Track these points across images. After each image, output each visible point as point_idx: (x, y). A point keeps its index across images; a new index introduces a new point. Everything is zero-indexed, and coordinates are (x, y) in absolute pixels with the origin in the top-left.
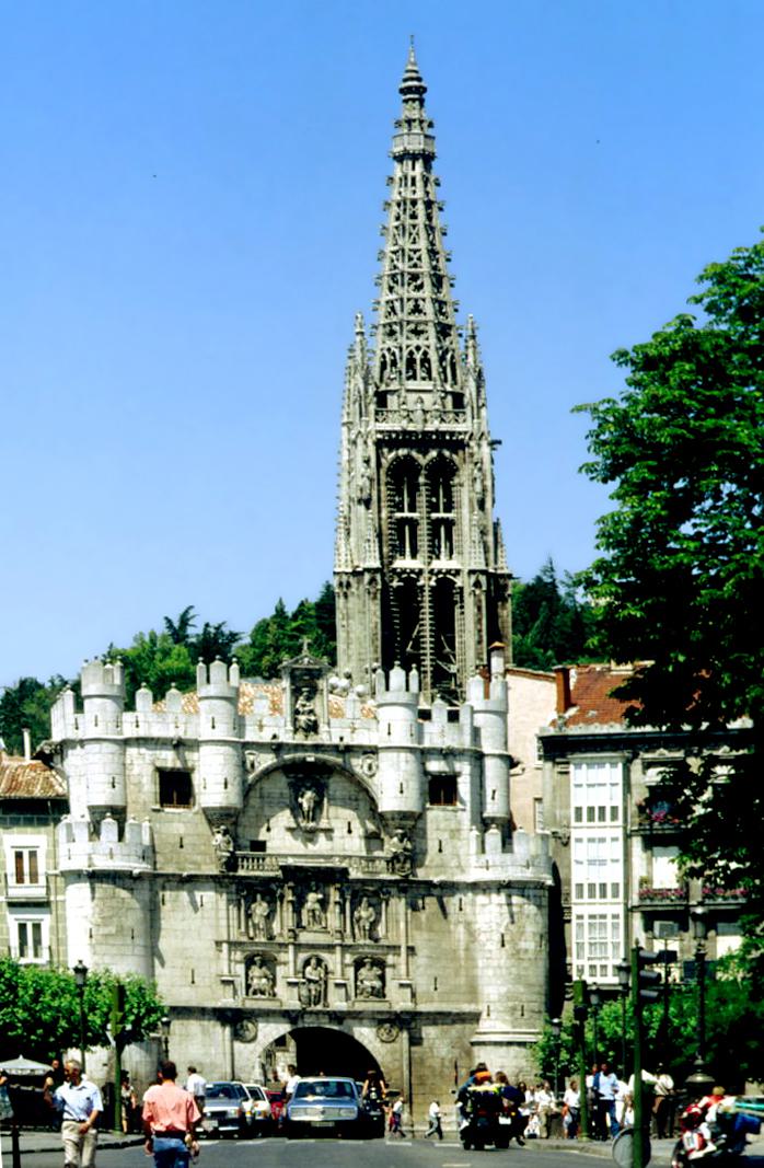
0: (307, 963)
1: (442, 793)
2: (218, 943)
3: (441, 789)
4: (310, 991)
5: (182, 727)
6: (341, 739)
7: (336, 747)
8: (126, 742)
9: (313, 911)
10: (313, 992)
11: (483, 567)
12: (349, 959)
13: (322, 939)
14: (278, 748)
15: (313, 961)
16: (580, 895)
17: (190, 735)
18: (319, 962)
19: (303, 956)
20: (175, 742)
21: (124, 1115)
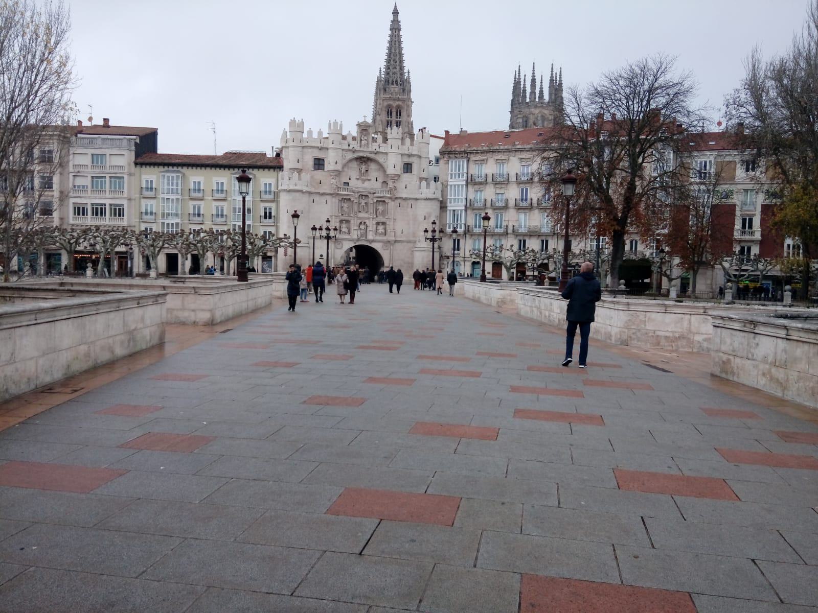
0: (361, 223)
1: (711, 143)
3: (408, 168)
5: (322, 143)
8: (303, 147)
12: (374, 222)
13: (366, 215)
16: (451, 203)
17: (325, 146)
18: (365, 223)
19: (359, 221)
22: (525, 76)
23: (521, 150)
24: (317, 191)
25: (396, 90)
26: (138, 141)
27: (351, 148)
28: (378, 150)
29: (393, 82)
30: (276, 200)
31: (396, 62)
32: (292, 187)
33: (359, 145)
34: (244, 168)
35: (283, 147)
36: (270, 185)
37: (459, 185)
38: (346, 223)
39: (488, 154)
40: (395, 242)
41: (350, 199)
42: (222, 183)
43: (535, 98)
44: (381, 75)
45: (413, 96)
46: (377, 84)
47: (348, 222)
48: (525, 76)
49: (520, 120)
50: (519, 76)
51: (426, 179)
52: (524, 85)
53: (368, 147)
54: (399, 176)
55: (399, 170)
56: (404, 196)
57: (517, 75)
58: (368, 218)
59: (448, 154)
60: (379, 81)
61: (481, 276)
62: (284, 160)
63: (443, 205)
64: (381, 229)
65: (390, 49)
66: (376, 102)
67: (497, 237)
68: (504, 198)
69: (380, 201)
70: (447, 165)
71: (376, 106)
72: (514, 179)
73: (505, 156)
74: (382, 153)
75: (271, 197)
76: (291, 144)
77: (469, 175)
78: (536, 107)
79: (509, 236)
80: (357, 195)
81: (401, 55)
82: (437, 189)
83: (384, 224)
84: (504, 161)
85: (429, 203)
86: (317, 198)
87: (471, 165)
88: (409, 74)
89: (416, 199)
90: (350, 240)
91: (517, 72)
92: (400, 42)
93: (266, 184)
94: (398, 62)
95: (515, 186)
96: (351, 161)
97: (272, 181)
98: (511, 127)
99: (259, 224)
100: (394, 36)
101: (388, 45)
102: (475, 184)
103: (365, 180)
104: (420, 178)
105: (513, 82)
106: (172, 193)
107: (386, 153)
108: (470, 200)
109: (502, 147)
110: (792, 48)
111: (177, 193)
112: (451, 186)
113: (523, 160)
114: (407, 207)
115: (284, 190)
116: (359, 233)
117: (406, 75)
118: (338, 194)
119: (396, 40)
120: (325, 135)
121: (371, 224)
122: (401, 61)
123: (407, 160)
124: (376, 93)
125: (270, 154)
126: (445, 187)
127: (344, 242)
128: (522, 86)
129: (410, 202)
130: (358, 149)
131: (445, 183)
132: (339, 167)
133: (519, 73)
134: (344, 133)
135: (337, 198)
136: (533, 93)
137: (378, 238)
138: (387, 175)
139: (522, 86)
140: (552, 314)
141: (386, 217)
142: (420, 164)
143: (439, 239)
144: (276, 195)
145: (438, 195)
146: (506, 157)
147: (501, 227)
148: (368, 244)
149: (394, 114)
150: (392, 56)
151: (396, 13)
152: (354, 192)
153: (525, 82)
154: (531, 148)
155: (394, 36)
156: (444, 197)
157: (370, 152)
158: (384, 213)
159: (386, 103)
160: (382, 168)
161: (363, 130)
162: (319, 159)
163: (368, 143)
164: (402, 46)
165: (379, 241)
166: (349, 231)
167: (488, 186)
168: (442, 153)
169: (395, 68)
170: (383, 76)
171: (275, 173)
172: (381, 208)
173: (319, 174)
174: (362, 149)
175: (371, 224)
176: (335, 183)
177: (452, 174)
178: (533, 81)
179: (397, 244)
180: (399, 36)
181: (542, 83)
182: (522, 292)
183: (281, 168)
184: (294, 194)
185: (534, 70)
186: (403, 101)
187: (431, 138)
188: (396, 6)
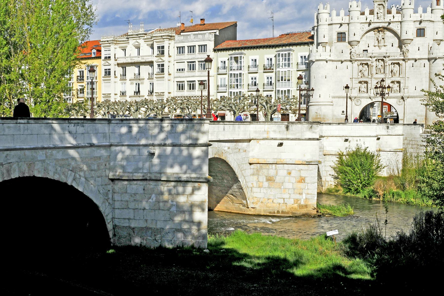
26: (218, 33)
69: (394, 64)
110: (315, 220)
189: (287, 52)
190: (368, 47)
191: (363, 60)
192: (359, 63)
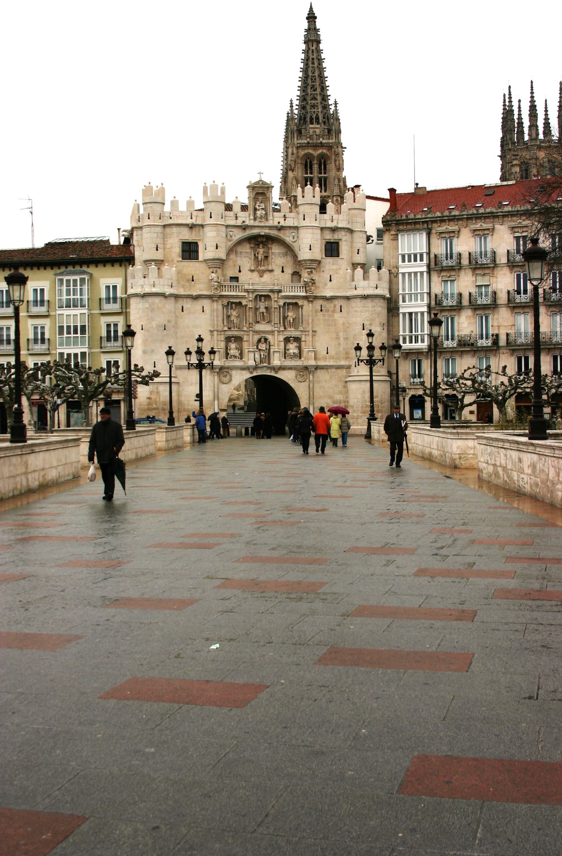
0: (259, 341)
2: (211, 331)
4: (260, 355)
6: (279, 223)
7: (276, 227)
8: (165, 226)
9: (263, 313)
10: (262, 356)
11: (339, 194)
12: (281, 338)
13: (268, 328)
14: (244, 228)
15: (263, 340)
16: (404, 301)
18: (266, 340)
19: (256, 337)
20: (190, 225)
21: (558, 280)
22: (519, 101)
23: (511, 214)
24: (187, 293)
25: (318, 131)
27: (239, 222)
28: (283, 223)
29: (311, 119)
30: (124, 312)
31: (315, 90)
32: (148, 290)
33: (252, 217)
34: (16, 266)
35: (133, 229)
36: (115, 287)
37: (416, 273)
38: (235, 341)
39: (460, 222)
40: (317, 368)
41: (240, 303)
42: (42, 291)
43: (538, 134)
44: (292, 110)
45: (345, 139)
46: (288, 124)
47: (239, 339)
48: (519, 101)
49: (517, 169)
50: (510, 102)
51: (363, 266)
52: (520, 115)
53: (267, 220)
54: (319, 262)
55: (318, 253)
56: (328, 294)
57: (507, 100)
58: (272, 332)
59: (396, 224)
60: (290, 119)
61: (168, 419)
62: (136, 249)
63: (393, 305)
64: (292, 348)
65: (305, 70)
66: (287, 152)
67: (482, 354)
68: (490, 290)
69: (289, 304)
70: (395, 242)
71: (286, 157)
72: (504, 260)
73: (452, 227)
74: (290, 227)
75: (116, 307)
76: (147, 222)
77: (432, 256)
78: (540, 148)
79: (501, 351)
80: (252, 296)
81: (322, 78)
82: (380, 279)
83: (297, 340)
84: (486, 232)
85: (369, 303)
86: (188, 305)
87: (435, 241)
88: (336, 106)
89: (348, 298)
90: (242, 369)
91: (507, 96)
92: (320, 61)
93: (108, 287)
94: (319, 90)
95: (506, 270)
96: (240, 242)
97: (118, 282)
98: (503, 178)
99: (98, 350)
100: (310, 52)
101: (302, 65)
102: (442, 270)
103: (264, 271)
104: (353, 264)
105: (502, 111)
106: (75, 306)
107: (296, 228)
108: (436, 295)
109: (481, 211)
111: (83, 306)
112: (404, 274)
113: (516, 230)
114: (334, 311)
115: (136, 295)
116: (257, 356)
117: (332, 107)
118: (221, 297)
119: (315, 57)
120: (199, 205)
121: (277, 342)
122: (324, 88)
123: (329, 236)
124: (286, 137)
125: (116, 240)
126: (393, 275)
127: (234, 373)
128: (516, 117)
129: (338, 303)
130: (252, 223)
131: (393, 271)
132: (222, 255)
133: (510, 98)
134: (229, 200)
135: (220, 302)
136: (533, 126)
137: (289, 363)
138: (300, 262)
139: (516, 117)
140: (522, 476)
141: (301, 328)
142: (352, 242)
143: (380, 360)
144: (125, 303)
145: (384, 291)
146: (490, 226)
147: (487, 338)
148: (273, 374)
149: (316, 167)
150: (309, 81)
151: (311, 17)
152: (247, 291)
153: (520, 111)
154: (527, 210)
155: (310, 52)
156: (393, 293)
157: (270, 228)
158: (296, 323)
159: (302, 153)
160: (289, 250)
161: (258, 194)
162: (190, 243)
163: (266, 214)
164: (324, 65)
165: (290, 368)
166: (300, 353)
167: (462, 273)
168: (386, 222)
169: (315, 99)
170: (296, 112)
171: (123, 269)
172: (291, 315)
173: (190, 267)
174: (257, 223)
175: (277, 342)
176: (216, 279)
177: (403, 256)
178: (533, 108)
179: (319, 373)
180: (319, 51)
181: (546, 111)
182: (484, 442)
183: (130, 260)
184: (151, 300)
185: (532, 93)
186: (330, 147)
187: (368, 201)
188: (311, 8)
189: (78, 278)
190: (240, 271)
191: (232, 297)
192: (225, 302)
